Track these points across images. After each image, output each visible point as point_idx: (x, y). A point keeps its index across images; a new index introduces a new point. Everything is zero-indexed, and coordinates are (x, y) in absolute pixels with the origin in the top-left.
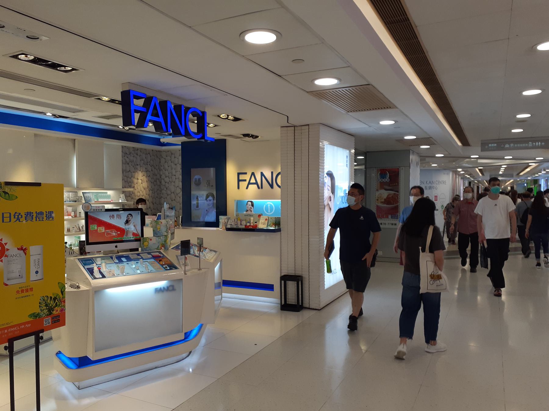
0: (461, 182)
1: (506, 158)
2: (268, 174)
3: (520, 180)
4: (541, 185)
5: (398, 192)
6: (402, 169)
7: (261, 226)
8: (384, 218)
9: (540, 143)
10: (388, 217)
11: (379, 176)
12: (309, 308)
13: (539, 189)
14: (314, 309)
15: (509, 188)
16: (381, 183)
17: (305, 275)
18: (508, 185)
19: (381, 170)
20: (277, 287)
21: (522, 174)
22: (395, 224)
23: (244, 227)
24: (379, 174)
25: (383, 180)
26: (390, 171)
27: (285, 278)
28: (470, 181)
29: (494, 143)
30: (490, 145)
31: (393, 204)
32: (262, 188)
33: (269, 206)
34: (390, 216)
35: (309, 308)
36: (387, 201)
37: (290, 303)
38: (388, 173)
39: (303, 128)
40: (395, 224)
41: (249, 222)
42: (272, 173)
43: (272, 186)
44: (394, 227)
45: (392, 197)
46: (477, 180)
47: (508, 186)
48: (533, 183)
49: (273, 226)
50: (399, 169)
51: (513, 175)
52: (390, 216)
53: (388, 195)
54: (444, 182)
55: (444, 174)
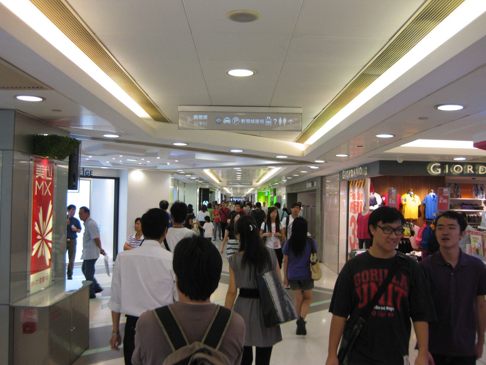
30: (196, 117)
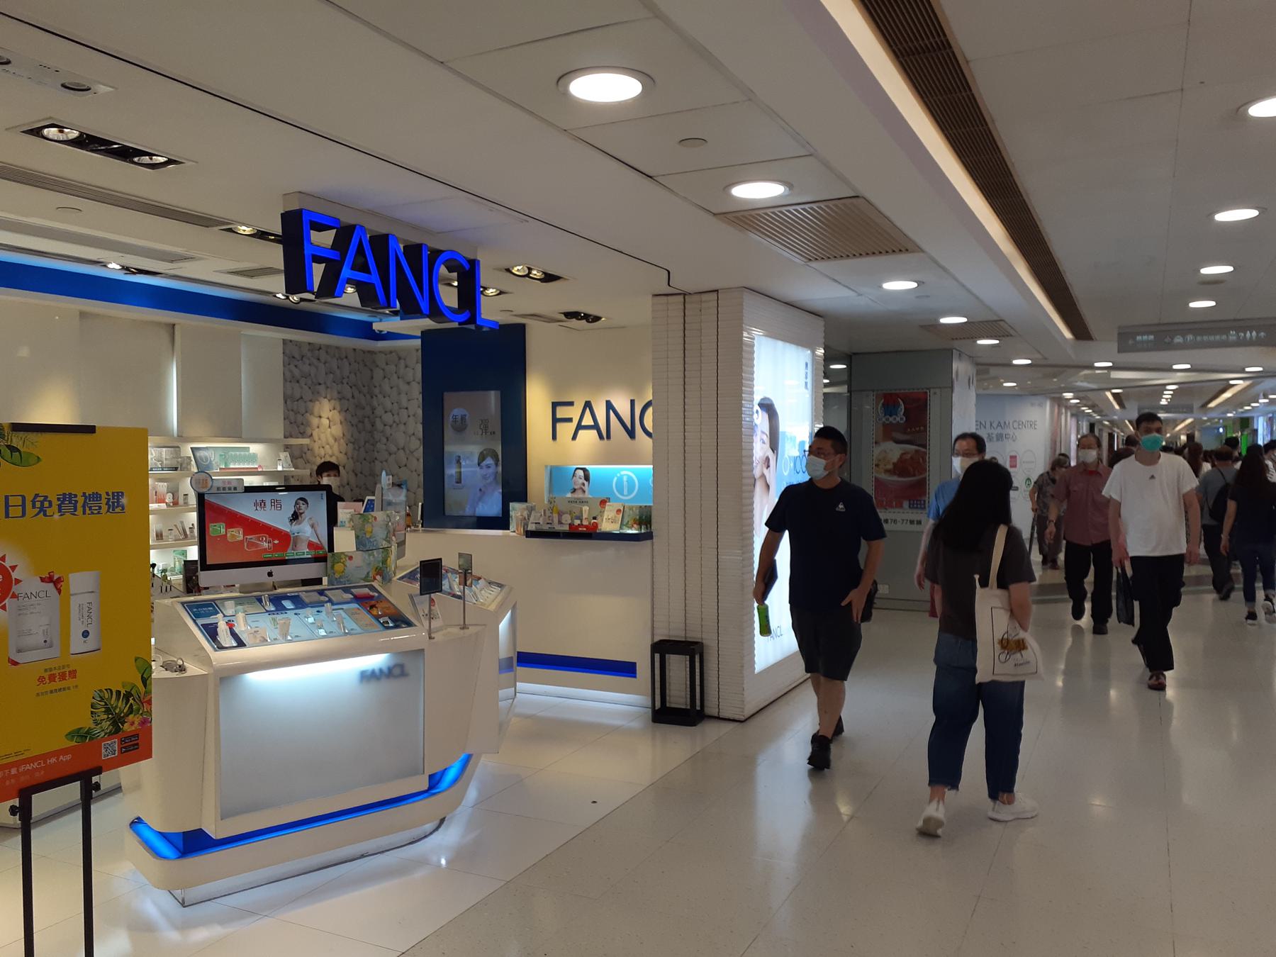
0: (1072, 423)
1: (1175, 367)
2: (622, 406)
3: (1209, 420)
4: (1256, 431)
5: (924, 446)
6: (935, 393)
7: (606, 526)
8: (891, 507)
9: (1254, 333)
10: (901, 506)
11: (880, 411)
12: (718, 718)
13: (1253, 441)
14: (729, 720)
15: (1184, 438)
16: (885, 425)
17: (709, 640)
18: (1180, 430)
19: (885, 396)
20: (643, 669)
21: (1212, 405)
22: (919, 522)
23: (566, 528)
24: (880, 405)
25: (891, 419)
26: (907, 399)
27: (662, 648)
28: (1092, 420)
29: (1148, 333)
30: (1139, 338)
31: (914, 475)
32: (609, 437)
33: (625, 479)
34: (906, 504)
35: (718, 718)
36: (901, 468)
37: (673, 706)
38: (901, 403)
39: (705, 297)
40: (919, 522)
41: (578, 518)
42: (632, 402)
43: (631, 433)
44: (915, 528)
45: (912, 458)
46: (1108, 418)
47: (1181, 434)
48: (1238, 426)
49: (635, 526)
50: (926, 393)
51: (1193, 407)
52: (906, 504)
53: (903, 454)
54: (1032, 425)
55: (1032, 405)
